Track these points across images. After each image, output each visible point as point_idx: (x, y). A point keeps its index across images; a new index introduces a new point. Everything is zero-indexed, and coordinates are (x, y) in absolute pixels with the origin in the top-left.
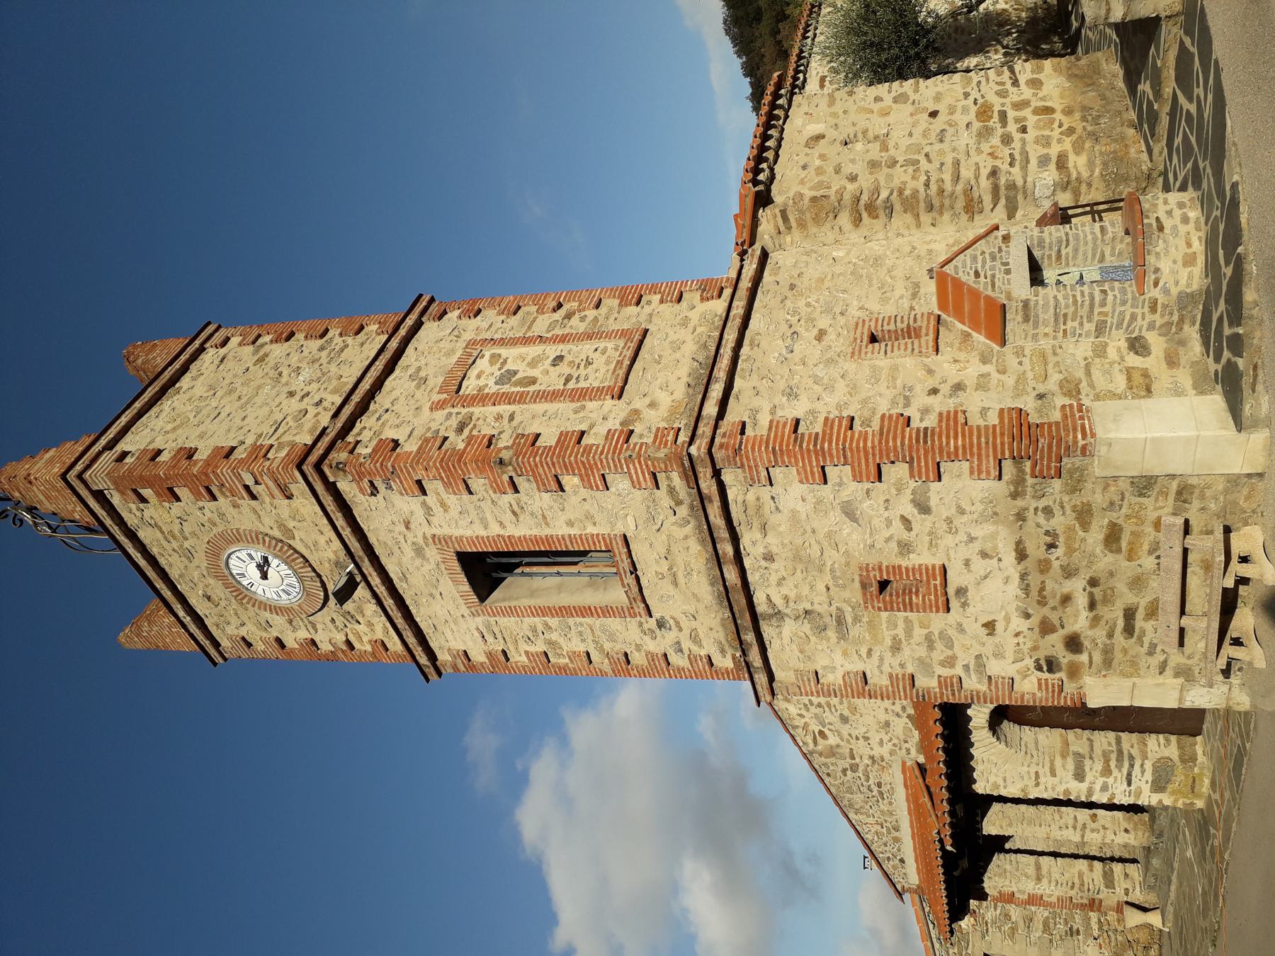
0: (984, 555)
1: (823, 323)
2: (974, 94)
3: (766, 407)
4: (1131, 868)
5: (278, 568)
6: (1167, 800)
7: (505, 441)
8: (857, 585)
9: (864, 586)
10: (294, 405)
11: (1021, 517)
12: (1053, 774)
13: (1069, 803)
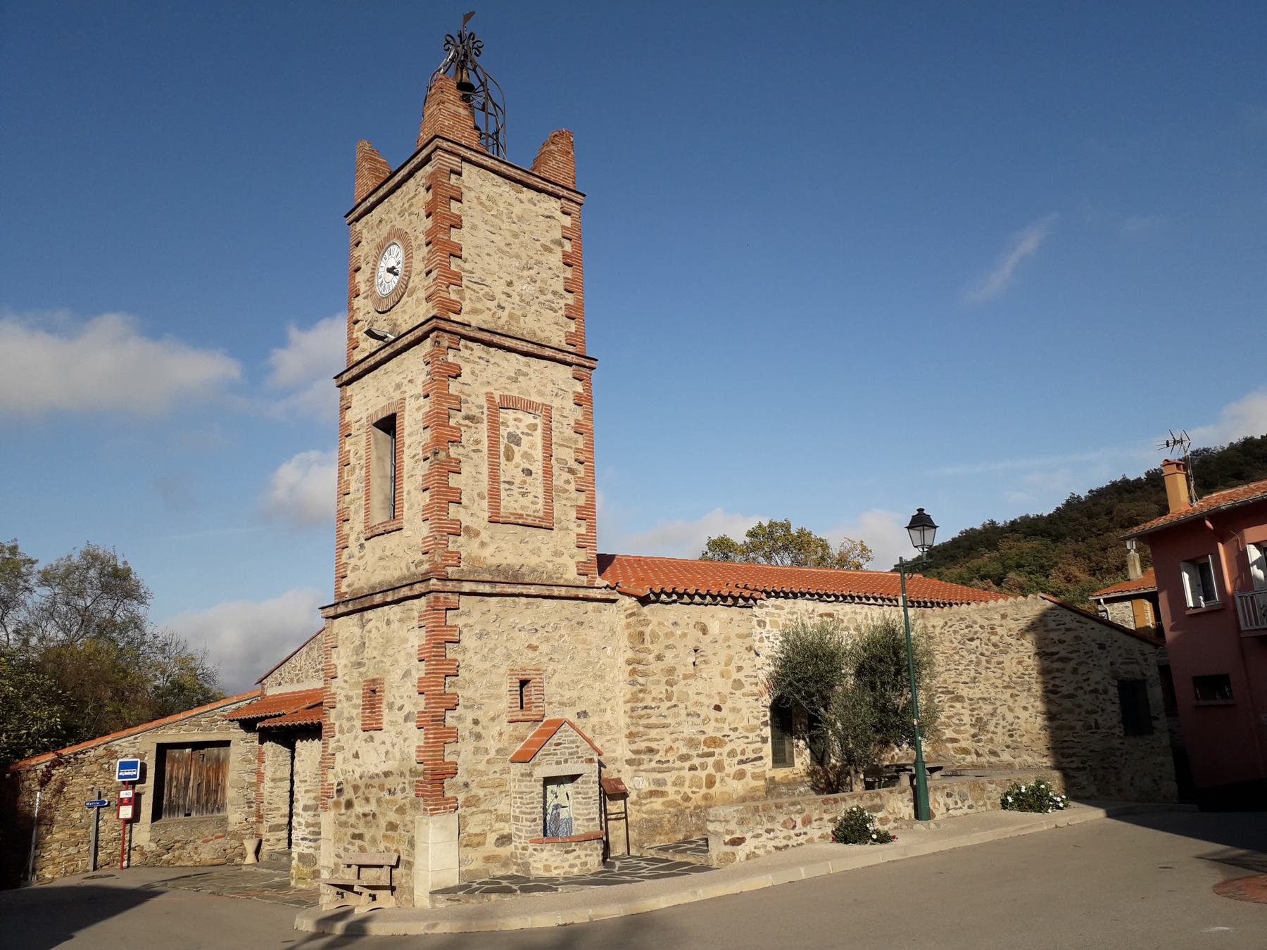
0: (387, 753)
1: (544, 648)
2: (733, 735)
3: (471, 621)
4: (285, 843)
5: (393, 281)
6: (294, 863)
7: (454, 451)
8: (376, 676)
9: (373, 680)
10: (499, 288)
11: (402, 774)
12: (306, 791)
13: (292, 802)
